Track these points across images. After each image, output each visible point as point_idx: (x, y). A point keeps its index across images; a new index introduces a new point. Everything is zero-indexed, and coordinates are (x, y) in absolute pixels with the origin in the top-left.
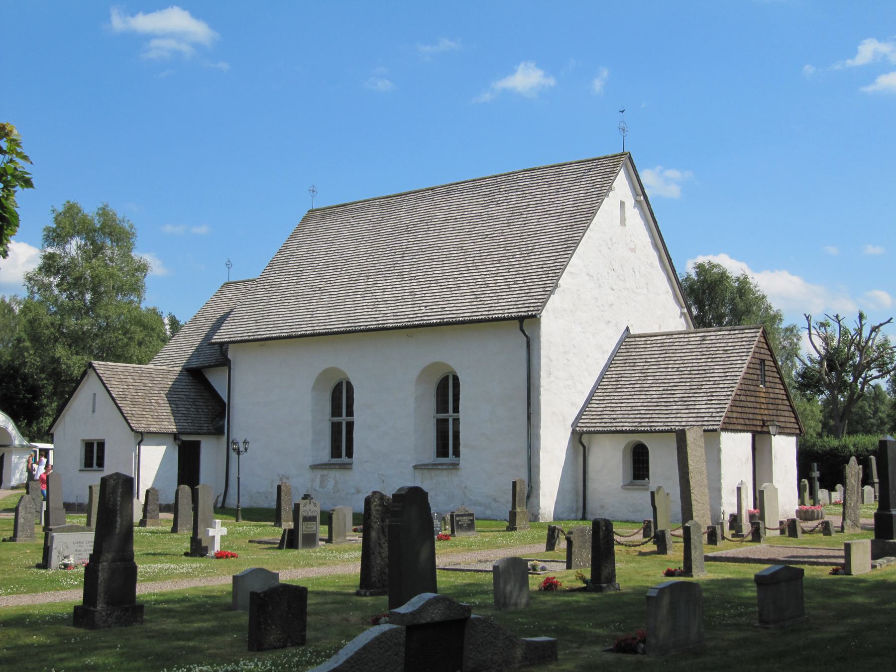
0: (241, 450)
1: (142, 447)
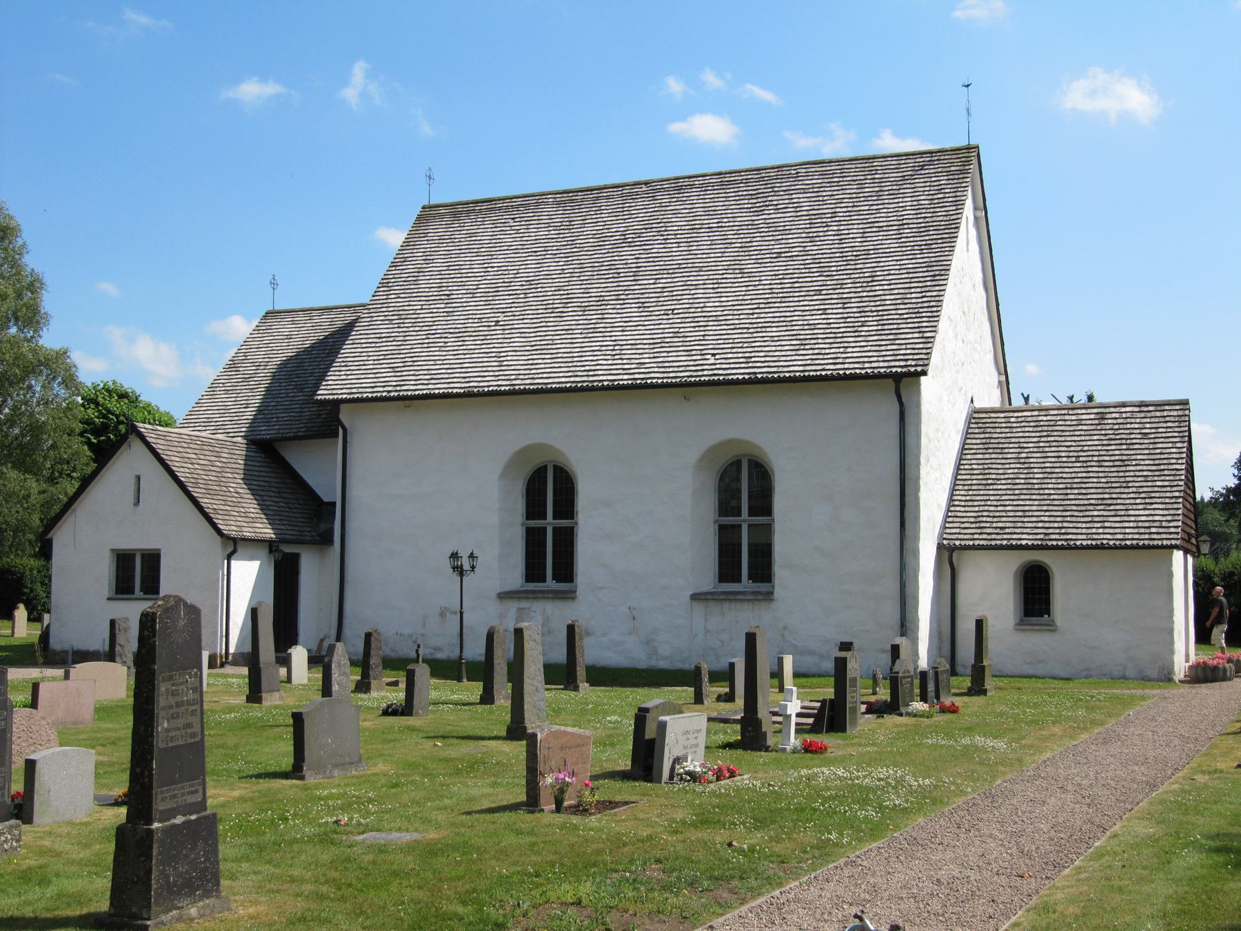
0: (465, 568)
1: (233, 563)
